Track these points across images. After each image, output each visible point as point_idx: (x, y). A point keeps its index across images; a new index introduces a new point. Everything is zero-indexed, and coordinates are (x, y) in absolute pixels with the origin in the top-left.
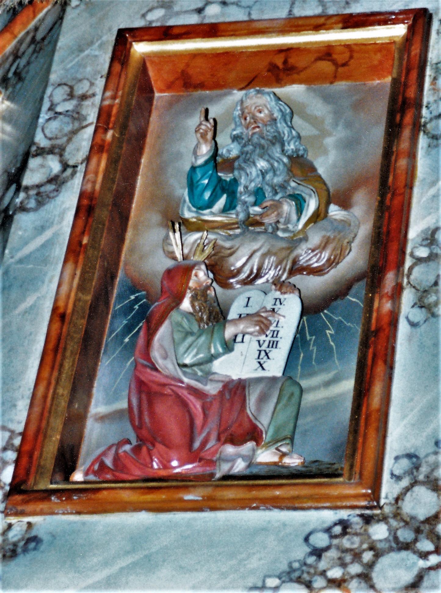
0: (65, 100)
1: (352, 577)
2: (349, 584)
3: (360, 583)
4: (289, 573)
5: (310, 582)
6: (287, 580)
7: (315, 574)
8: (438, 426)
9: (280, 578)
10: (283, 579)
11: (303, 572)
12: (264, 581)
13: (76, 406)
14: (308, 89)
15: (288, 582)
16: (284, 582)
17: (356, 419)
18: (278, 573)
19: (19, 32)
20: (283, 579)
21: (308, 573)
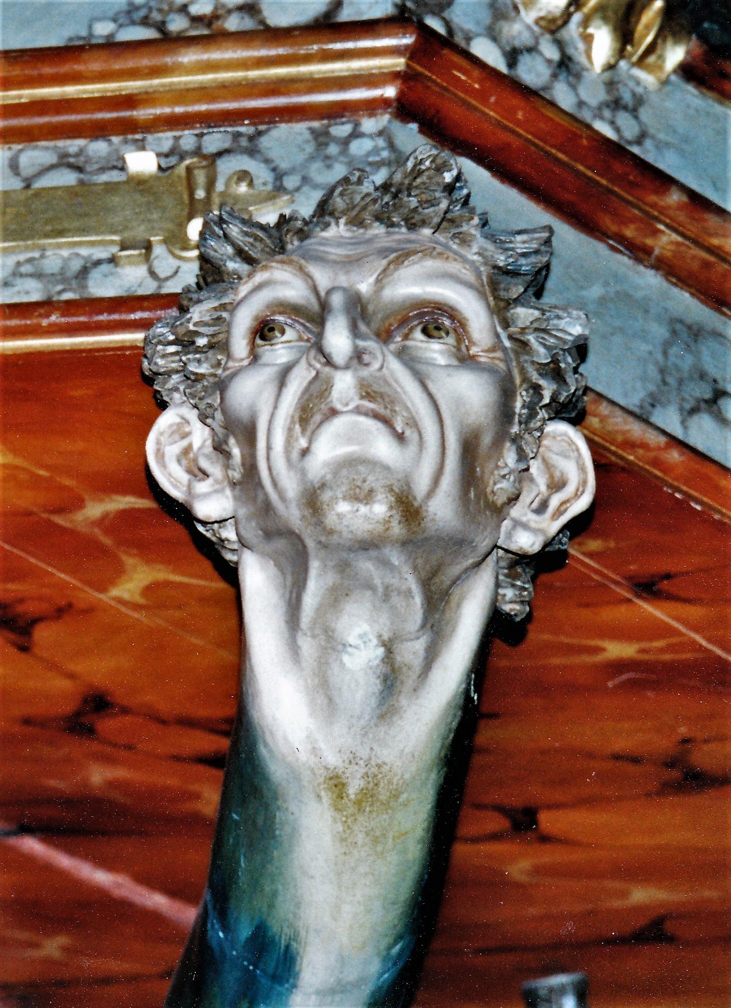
0: (540, 53)
1: (230, 12)
2: (224, 22)
3: (243, 18)
4: (129, 12)
5: (164, 23)
6: (127, 22)
7: (171, 10)
8: (725, 200)
9: (114, 20)
10: (121, 21)
11: (150, 9)
12: (90, 27)
13: (77, 393)
14: (265, 1003)
15: (127, 25)
16: (121, 26)
17: (515, 113)
18: (111, 14)
19: (594, 580)
20: (121, 21)
21: (160, 10)
